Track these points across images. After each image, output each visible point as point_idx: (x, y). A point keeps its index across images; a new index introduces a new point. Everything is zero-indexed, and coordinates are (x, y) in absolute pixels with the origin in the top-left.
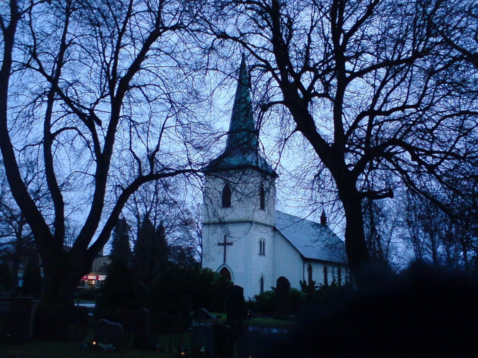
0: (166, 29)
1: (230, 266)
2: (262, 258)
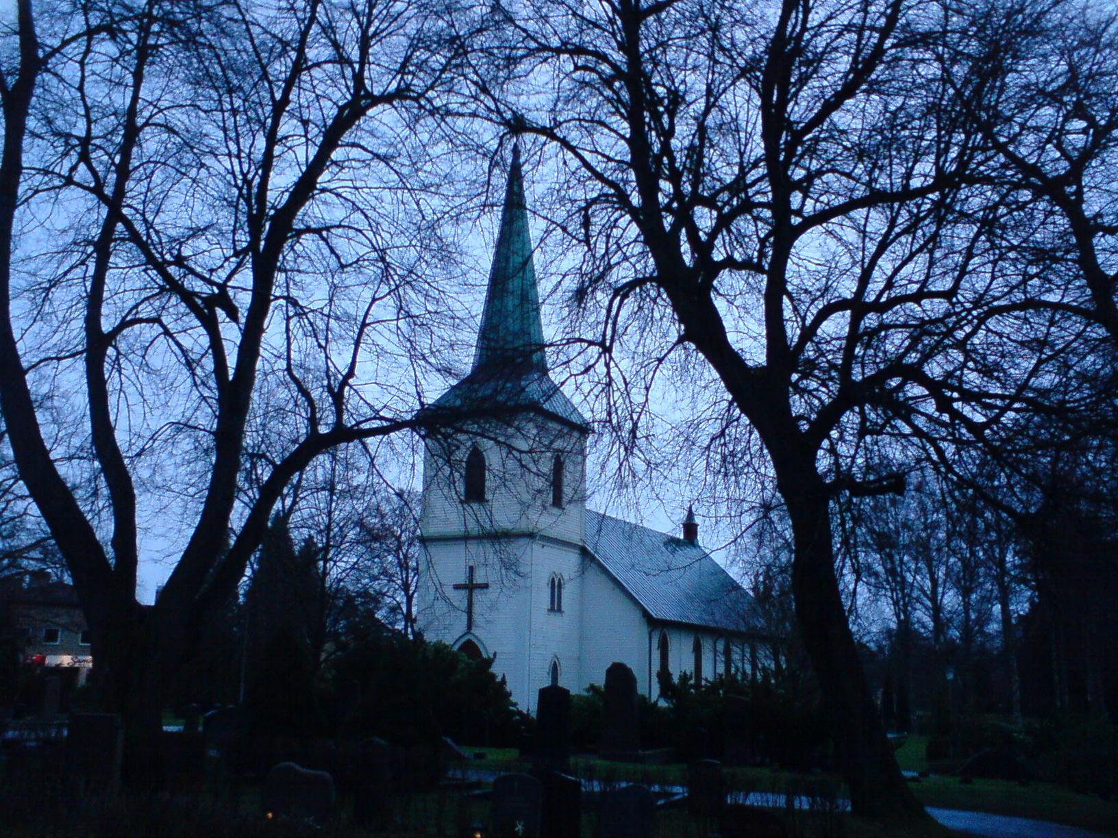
0: (375, 100)
1: (482, 638)
2: (554, 618)
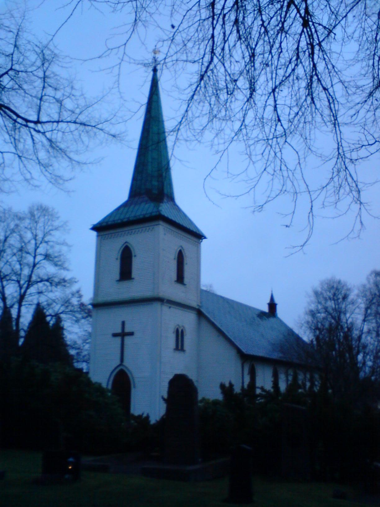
2: (179, 355)
